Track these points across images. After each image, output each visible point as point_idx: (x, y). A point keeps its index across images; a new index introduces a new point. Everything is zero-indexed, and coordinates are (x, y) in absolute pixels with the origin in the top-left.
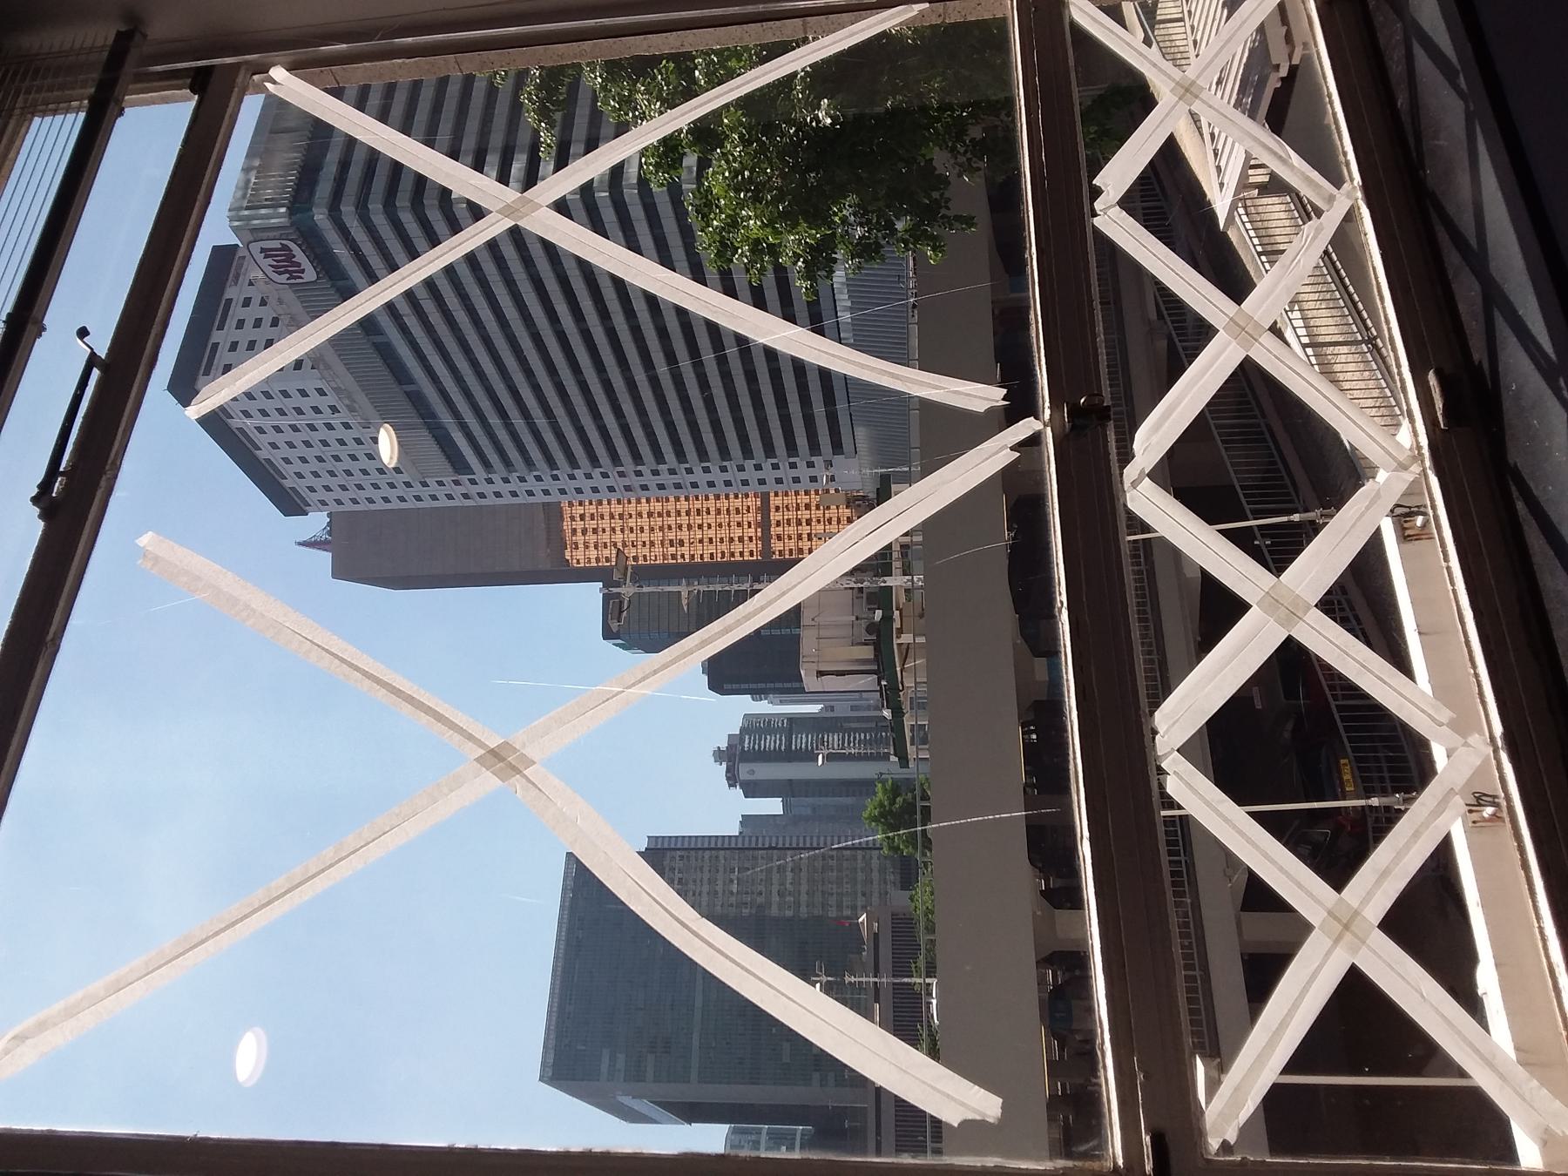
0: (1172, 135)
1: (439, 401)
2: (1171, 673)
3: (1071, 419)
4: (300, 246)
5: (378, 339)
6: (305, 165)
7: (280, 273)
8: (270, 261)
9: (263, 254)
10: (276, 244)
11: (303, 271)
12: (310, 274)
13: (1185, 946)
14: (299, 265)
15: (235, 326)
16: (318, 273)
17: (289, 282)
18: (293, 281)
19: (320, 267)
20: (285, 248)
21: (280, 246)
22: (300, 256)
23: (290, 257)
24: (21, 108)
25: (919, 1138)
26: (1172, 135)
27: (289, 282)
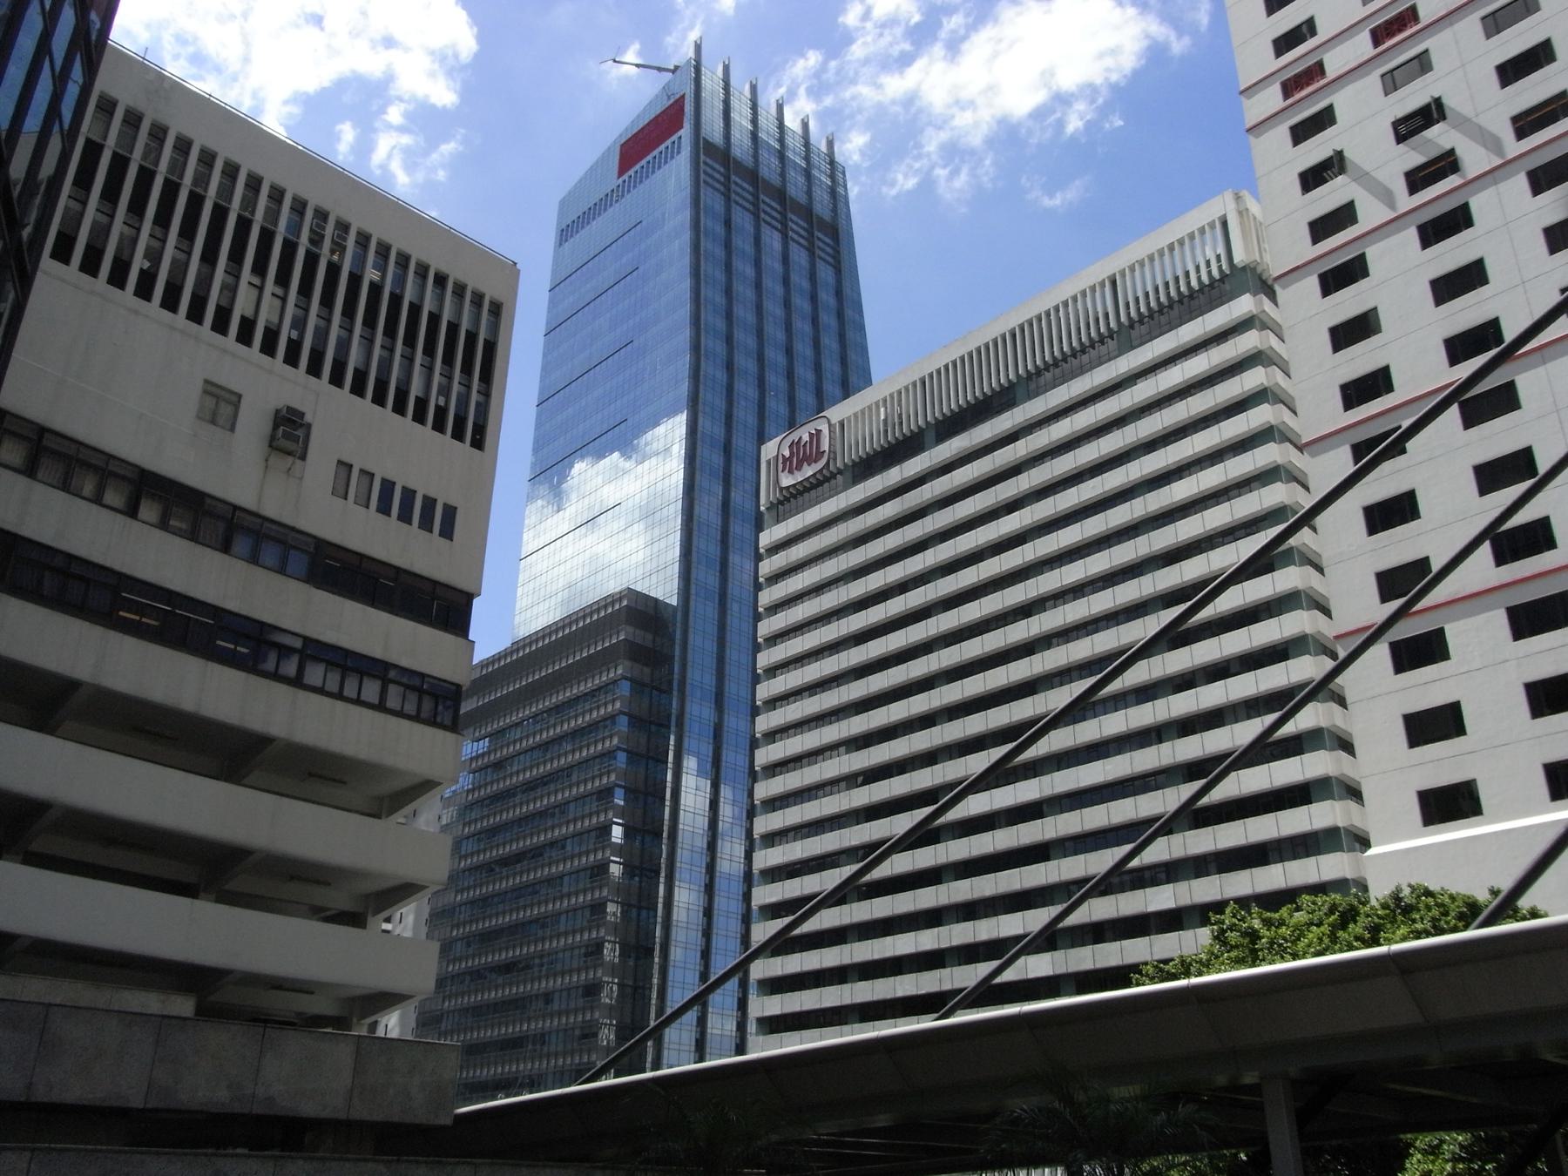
0: (1352, 202)
1: (1133, 365)
2: (1320, 696)
3: (651, 927)
4: (821, 470)
5: (930, 436)
6: (917, 434)
7: (791, 447)
8: (806, 437)
9: (814, 432)
10: (825, 446)
11: (791, 472)
12: (787, 481)
13: (229, 402)
14: (799, 468)
15: (686, 97)
16: (788, 488)
17: (780, 457)
18: (781, 460)
19: (808, 485)
20: (820, 454)
21: (822, 450)
22: (809, 471)
23: (810, 460)
24: (714, 376)
25: (882, 410)
26: (1352, 202)
27: (780, 457)
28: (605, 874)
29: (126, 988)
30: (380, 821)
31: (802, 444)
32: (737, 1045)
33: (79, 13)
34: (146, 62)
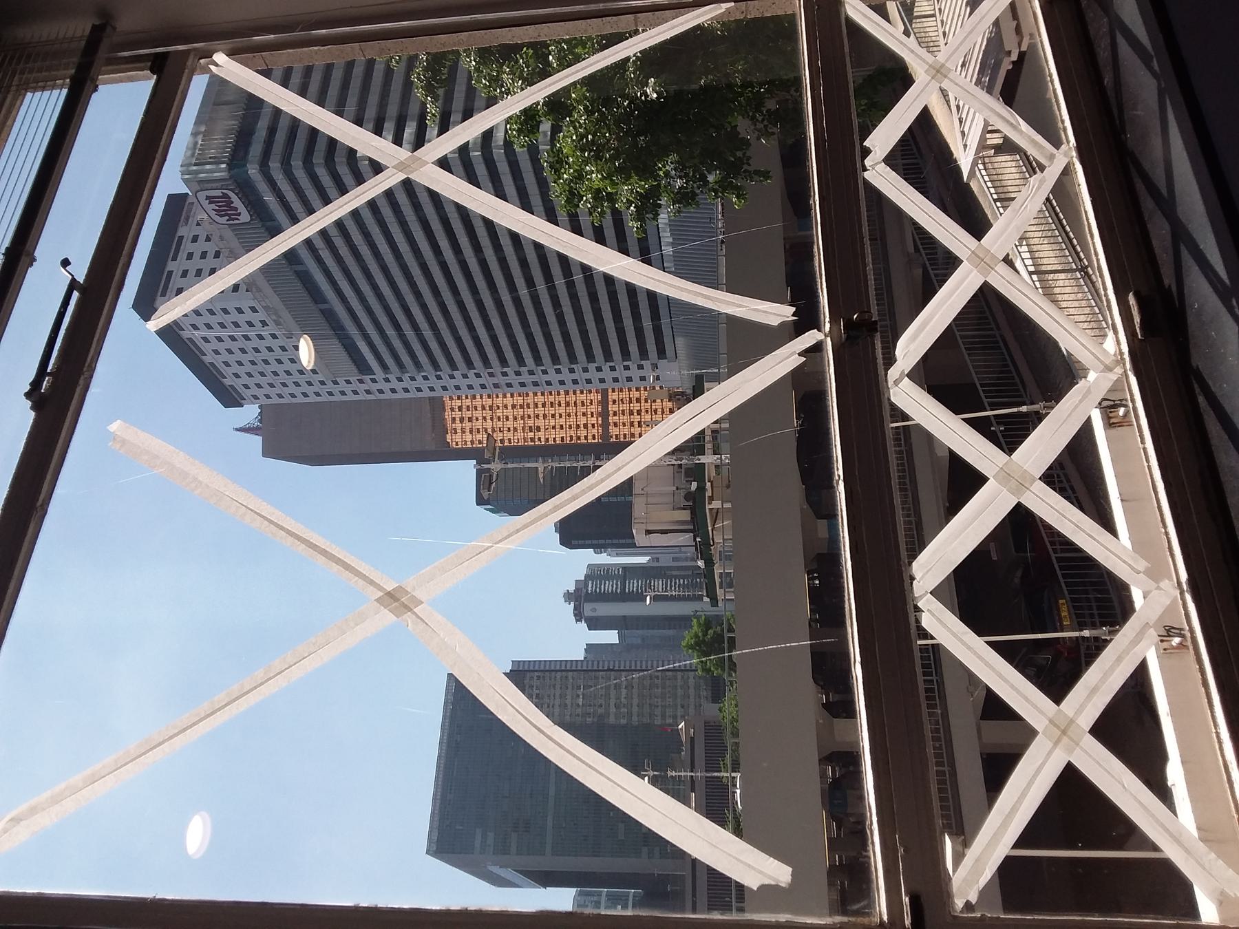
0: (926, 106)
4: (237, 194)
6: (241, 130)
7: (221, 216)
8: (213, 206)
9: (208, 201)
10: (218, 193)
11: (239, 214)
12: (245, 217)
14: (236, 209)
16: (251, 216)
17: (228, 222)
18: (231, 222)
20: (225, 196)
21: (221, 195)
22: (237, 202)
23: (229, 203)
26: (926, 106)
27: (228, 222)
28: (842, 912)
29: (952, 907)
30: (1015, 35)
31: (217, 208)
32: (312, 71)
33: (811, 170)
34: (1050, 84)
